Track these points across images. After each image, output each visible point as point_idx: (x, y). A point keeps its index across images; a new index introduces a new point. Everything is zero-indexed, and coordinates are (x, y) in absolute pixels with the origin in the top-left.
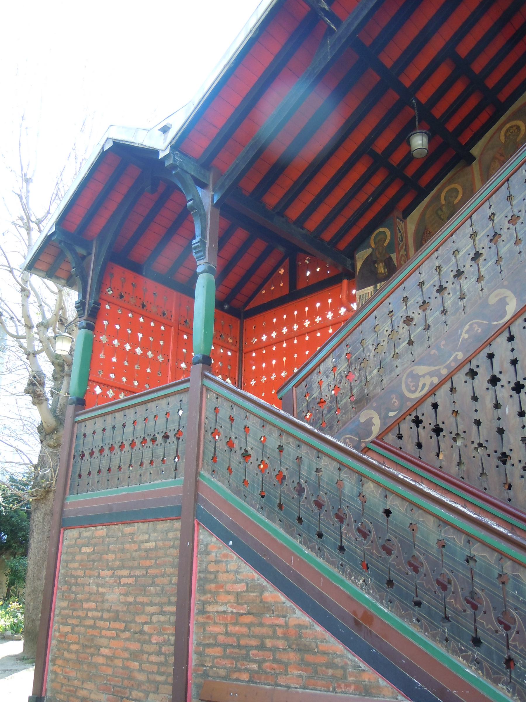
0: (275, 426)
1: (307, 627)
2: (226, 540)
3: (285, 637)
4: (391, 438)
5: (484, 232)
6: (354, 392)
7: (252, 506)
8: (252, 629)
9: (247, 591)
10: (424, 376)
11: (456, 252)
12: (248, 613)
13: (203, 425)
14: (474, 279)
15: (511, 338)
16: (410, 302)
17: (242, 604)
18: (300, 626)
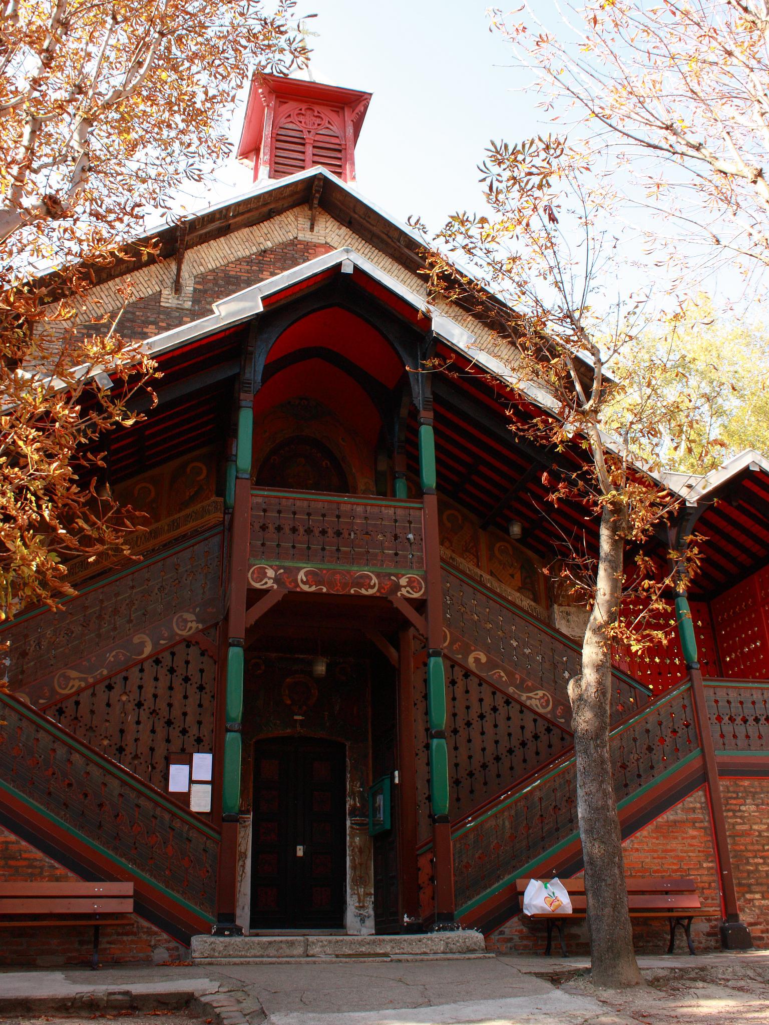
1: (13, 843)
10: (74, 679)
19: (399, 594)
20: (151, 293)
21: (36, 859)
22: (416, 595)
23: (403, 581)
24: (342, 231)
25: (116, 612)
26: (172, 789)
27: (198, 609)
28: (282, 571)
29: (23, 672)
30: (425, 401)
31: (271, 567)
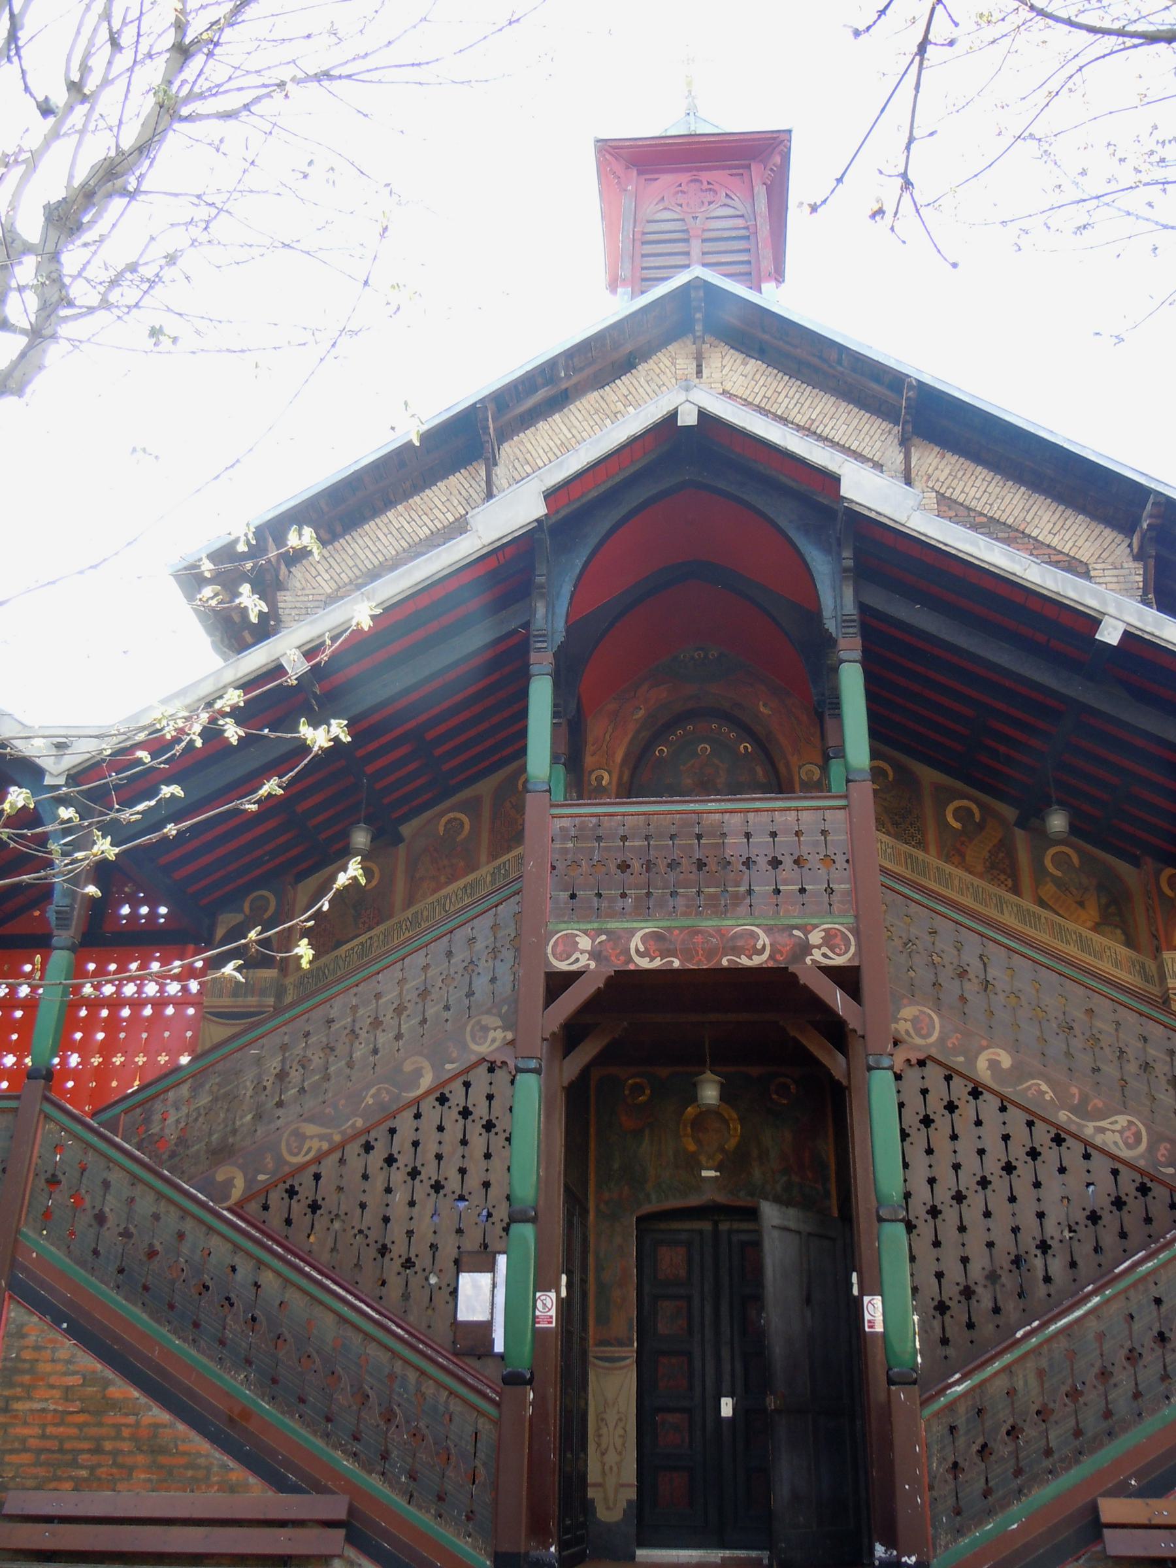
0: (151, 1187)
1: (165, 1426)
2: (57, 1322)
3: (133, 1438)
4: (253, 1207)
5: (414, 983)
6: (215, 1137)
7: (102, 1282)
8: (85, 1430)
9: (83, 1385)
10: (312, 1137)
11: (378, 996)
12: (82, 1411)
13: (33, 1166)
14: (391, 1035)
15: (418, 1116)
16: (313, 1040)
17: (73, 1401)
18: (156, 1426)
19: (808, 960)
20: (451, 519)
21: (200, 1455)
22: (839, 961)
23: (815, 937)
24: (749, 367)
25: (376, 1023)
26: (462, 1316)
27: (505, 1009)
28: (603, 937)
29: (234, 1132)
30: (846, 621)
31: (585, 932)
